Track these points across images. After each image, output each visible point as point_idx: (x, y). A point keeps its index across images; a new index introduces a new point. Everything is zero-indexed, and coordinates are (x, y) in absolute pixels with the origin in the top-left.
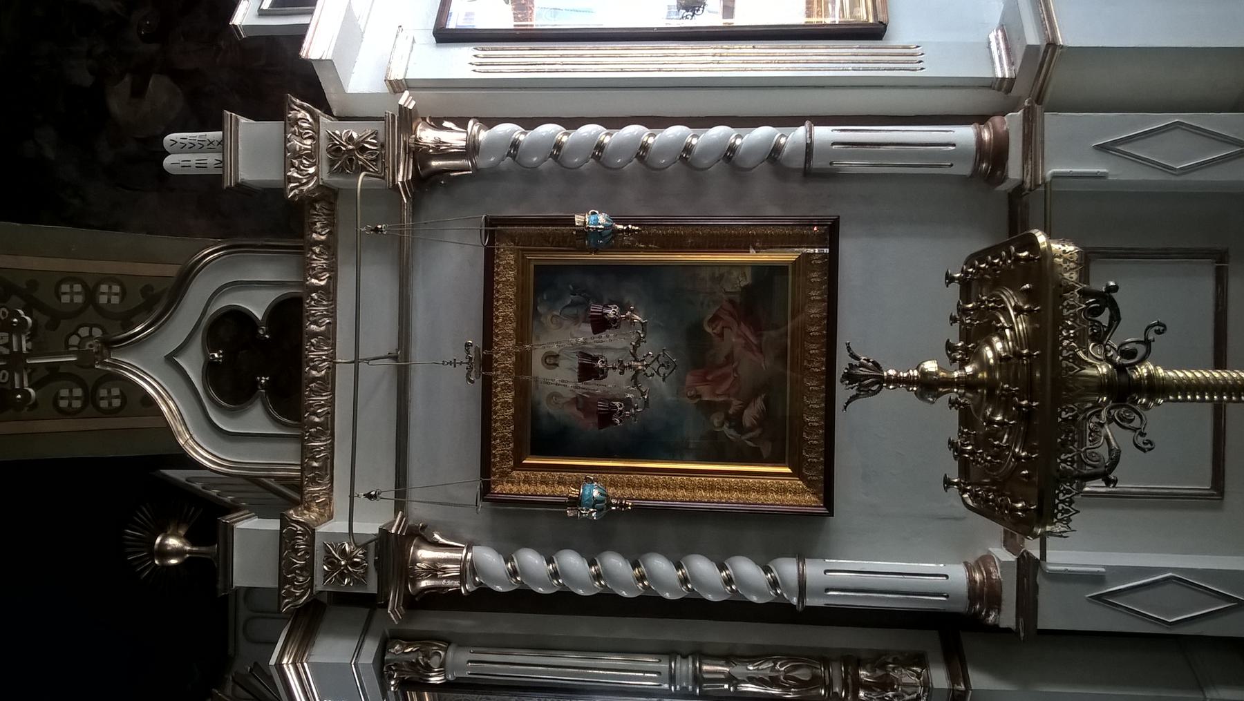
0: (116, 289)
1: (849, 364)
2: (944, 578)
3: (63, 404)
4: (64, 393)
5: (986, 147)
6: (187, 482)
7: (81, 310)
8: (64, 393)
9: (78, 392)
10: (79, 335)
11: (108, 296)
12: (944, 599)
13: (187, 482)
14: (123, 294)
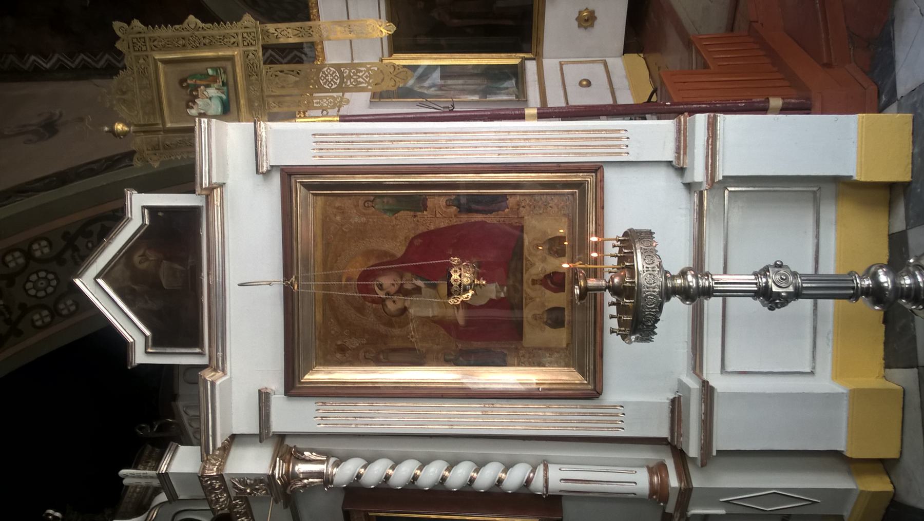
0: (44, 243)
1: (657, 328)
2: (634, 484)
3: (39, 323)
4: (36, 317)
5: (656, 487)
6: (465, 218)
7: (26, 266)
8: (36, 317)
9: (45, 313)
10: (31, 281)
11: (40, 250)
12: (428, 100)
13: (465, 218)
14: (50, 244)
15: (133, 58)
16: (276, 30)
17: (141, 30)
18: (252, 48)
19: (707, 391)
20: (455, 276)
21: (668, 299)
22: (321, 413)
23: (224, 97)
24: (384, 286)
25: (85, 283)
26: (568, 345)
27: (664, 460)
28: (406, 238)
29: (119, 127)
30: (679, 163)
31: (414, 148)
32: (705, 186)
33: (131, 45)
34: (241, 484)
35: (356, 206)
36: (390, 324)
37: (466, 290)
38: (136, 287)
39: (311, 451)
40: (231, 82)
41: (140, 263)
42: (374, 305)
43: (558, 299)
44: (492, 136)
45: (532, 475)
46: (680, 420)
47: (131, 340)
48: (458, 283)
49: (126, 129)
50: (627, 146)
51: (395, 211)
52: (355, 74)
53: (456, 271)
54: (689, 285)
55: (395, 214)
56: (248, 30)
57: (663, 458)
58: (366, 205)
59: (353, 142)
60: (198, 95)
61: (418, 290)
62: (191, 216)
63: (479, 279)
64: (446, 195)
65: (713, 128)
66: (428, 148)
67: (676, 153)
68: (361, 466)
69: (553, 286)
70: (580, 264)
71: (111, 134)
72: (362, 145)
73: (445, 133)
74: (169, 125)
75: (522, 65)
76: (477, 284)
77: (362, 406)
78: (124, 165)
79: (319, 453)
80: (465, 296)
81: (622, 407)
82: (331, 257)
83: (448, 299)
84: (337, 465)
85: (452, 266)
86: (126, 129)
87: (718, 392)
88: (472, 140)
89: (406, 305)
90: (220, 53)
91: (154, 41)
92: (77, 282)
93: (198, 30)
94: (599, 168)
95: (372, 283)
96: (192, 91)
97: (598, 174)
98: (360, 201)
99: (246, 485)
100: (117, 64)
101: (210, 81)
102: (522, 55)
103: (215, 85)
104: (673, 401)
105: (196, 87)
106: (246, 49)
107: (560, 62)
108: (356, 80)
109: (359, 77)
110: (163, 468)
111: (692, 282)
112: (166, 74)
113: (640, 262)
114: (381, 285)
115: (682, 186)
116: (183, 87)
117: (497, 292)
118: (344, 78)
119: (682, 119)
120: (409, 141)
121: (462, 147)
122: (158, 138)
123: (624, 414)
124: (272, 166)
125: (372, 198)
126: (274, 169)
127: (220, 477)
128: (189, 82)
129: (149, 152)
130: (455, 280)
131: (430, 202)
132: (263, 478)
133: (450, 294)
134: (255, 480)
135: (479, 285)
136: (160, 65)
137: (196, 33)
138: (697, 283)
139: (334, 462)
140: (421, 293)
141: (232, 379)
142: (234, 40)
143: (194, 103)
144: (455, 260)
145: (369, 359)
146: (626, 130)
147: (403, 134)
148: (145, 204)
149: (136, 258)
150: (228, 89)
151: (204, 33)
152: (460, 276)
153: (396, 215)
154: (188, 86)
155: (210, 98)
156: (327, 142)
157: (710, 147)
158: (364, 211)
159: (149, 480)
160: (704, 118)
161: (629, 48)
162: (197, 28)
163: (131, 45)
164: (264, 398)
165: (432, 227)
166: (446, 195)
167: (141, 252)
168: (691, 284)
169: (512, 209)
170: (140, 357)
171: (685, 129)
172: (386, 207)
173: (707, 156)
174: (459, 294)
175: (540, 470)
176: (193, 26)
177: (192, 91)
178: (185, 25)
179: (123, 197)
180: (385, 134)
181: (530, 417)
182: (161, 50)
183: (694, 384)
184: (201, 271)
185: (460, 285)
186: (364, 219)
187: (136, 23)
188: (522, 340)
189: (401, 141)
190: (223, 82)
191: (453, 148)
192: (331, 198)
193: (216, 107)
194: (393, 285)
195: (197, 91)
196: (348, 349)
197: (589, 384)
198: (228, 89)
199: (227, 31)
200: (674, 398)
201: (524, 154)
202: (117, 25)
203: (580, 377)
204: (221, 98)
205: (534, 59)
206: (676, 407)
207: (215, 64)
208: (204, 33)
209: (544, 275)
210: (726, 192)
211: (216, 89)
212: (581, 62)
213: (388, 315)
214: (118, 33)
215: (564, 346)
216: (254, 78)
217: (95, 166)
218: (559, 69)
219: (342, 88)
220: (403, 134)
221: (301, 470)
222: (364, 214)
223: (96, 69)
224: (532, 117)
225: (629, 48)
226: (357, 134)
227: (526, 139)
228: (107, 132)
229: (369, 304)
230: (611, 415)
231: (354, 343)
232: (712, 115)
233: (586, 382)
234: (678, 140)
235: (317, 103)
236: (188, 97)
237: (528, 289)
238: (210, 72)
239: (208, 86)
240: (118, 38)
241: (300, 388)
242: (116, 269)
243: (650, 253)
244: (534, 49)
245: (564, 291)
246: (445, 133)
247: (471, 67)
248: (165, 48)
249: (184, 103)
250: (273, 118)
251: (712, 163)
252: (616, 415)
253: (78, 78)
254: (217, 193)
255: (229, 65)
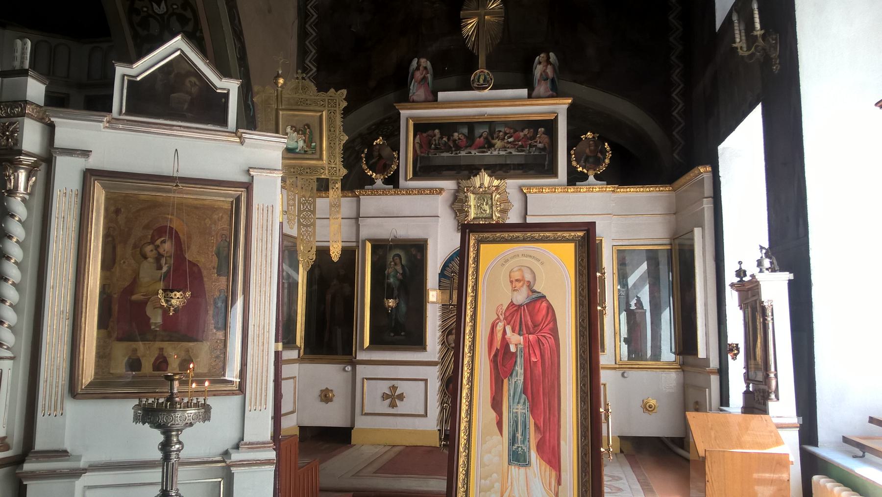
15: (324, 98)
16: (337, 188)
17: (341, 106)
18: (327, 172)
19: (76, 473)
20: (178, 294)
21: (163, 433)
22: (68, 192)
23: (297, 151)
24: (164, 244)
25: (177, 41)
26: (112, 374)
27: (11, 449)
28: (198, 261)
29: (281, 81)
30: (242, 445)
31: (261, 270)
32: (228, 461)
33: (332, 98)
34: (13, 128)
35: (223, 229)
36: (135, 247)
37: (167, 301)
38: (172, 76)
39: (35, 182)
40: (307, 156)
41: (190, 81)
42: (150, 236)
43: (147, 367)
44: (267, 321)
45: (5, 347)
46: (49, 457)
47: (135, 66)
48: (173, 297)
49: (280, 85)
50: (255, 410)
51: (218, 254)
52: (309, 234)
53: (181, 295)
54: (172, 446)
55: (216, 255)
56: (338, 171)
57: (13, 448)
58: (223, 236)
59: (267, 230)
60: (299, 134)
61: (160, 268)
62: (221, 120)
63: (174, 310)
64: (227, 289)
65: (267, 463)
66: (261, 278)
67: (249, 443)
68: (21, 218)
69: (158, 362)
70: (192, 375)
71: (276, 75)
72: (265, 236)
73: (270, 290)
74: (281, 113)
75: (296, 348)
76: (170, 309)
77: (73, 223)
78: (236, 43)
79: (33, 186)
80: (163, 301)
81: (62, 415)
82: (181, 208)
83: (162, 290)
84: (24, 200)
85: (184, 293)
86: (280, 85)
87: (74, 482)
88: (265, 308)
89: (149, 259)
90: (324, 152)
91: (334, 113)
92: (179, 37)
93: (339, 140)
94: (242, 392)
95: (167, 236)
96: (302, 131)
97: (238, 391)
98: (226, 232)
99: (13, 132)
100: (308, 41)
101: (308, 142)
102: (303, 347)
103: (305, 146)
104: (66, 452)
105: (304, 134)
106: (327, 168)
107: (296, 377)
108: (305, 234)
109: (307, 237)
110: (30, 73)
111: (175, 448)
112: (312, 116)
113: (192, 412)
114: (165, 242)
115: (226, 449)
116: (305, 126)
117: (156, 323)
118: (307, 227)
119: (271, 445)
120: (266, 266)
121: (260, 301)
122: (273, 104)
123: (56, 416)
124: (253, 177)
125: (228, 240)
126: (251, 178)
127: (23, 114)
128: (308, 130)
129: (263, 97)
130: (175, 295)
131: (223, 279)
132: (18, 145)
133: (165, 290)
134: (17, 140)
135: (170, 311)
136: (319, 114)
137: (338, 139)
138: (174, 451)
139: (26, 199)
140: (157, 270)
141: (99, 132)
142: (332, 162)
143: (295, 131)
144: (188, 294)
145: (109, 229)
146: (266, 408)
147: (271, 263)
148: (231, 92)
149: (193, 79)
150: (302, 154)
151: (337, 143)
152: (178, 298)
153: (215, 255)
154: (306, 129)
155: (297, 142)
156: (267, 213)
157: (254, 462)
158: (219, 234)
159: (19, 59)
160: (273, 457)
161: (302, 429)
162: (340, 140)
163: (332, 98)
164: (86, 153)
165: (205, 279)
166: (227, 289)
167: (197, 83)
168: (173, 447)
169: (216, 334)
170: (120, 70)
171: (265, 447)
172: (221, 249)
173: (248, 461)
174: (164, 297)
175: (9, 354)
176: (342, 137)
177: (302, 131)
178: (343, 133)
179: (237, 78)
180: (271, 251)
181: (57, 346)
182: (328, 116)
183: (82, 464)
184: (182, 121)
185: (172, 298)
186: (213, 233)
187: (345, 104)
188: (117, 341)
189: (266, 261)
190: (307, 151)
191: (260, 296)
192: (229, 213)
193: (292, 145)
194: (164, 251)
195: (302, 134)
196: (117, 215)
197: (82, 389)
198: (302, 154)
199: (337, 159)
200: (68, 452)
201: (253, 342)
202: (344, 92)
203: (88, 383)
204: (297, 148)
205: (299, 357)
206: (62, 454)
207: (318, 148)
208: (337, 143)
209: (166, 356)
210: (220, 480)
211: (303, 146)
212: (295, 393)
213: (142, 245)
214: (339, 92)
215: (111, 372)
216: (308, 171)
217: (237, 21)
218: (291, 376)
219: (300, 224)
220: (271, 263)
221: (20, 174)
222: (217, 234)
223: (305, 23)
224: (276, 347)
225: (302, 429)
226: (272, 234)
227: (263, 344)
228: (278, 72)
229: (151, 234)
230: (56, 406)
231: (121, 219)
232: (275, 462)
233: (83, 387)
234: (258, 443)
235: (291, 208)
236: (298, 127)
237: (158, 344)
238: (313, 144)
239: (305, 141)
240: (337, 91)
241: (91, 179)
242: (186, 64)
243: (197, 418)
244: (307, 356)
245: (153, 371)
246: (270, 290)
247: (296, 308)
248: (329, 118)
249: (295, 125)
250: (283, 180)
251: (244, 464)
252: (55, 410)
253: (299, 9)
254: (238, 140)
255: (317, 156)
